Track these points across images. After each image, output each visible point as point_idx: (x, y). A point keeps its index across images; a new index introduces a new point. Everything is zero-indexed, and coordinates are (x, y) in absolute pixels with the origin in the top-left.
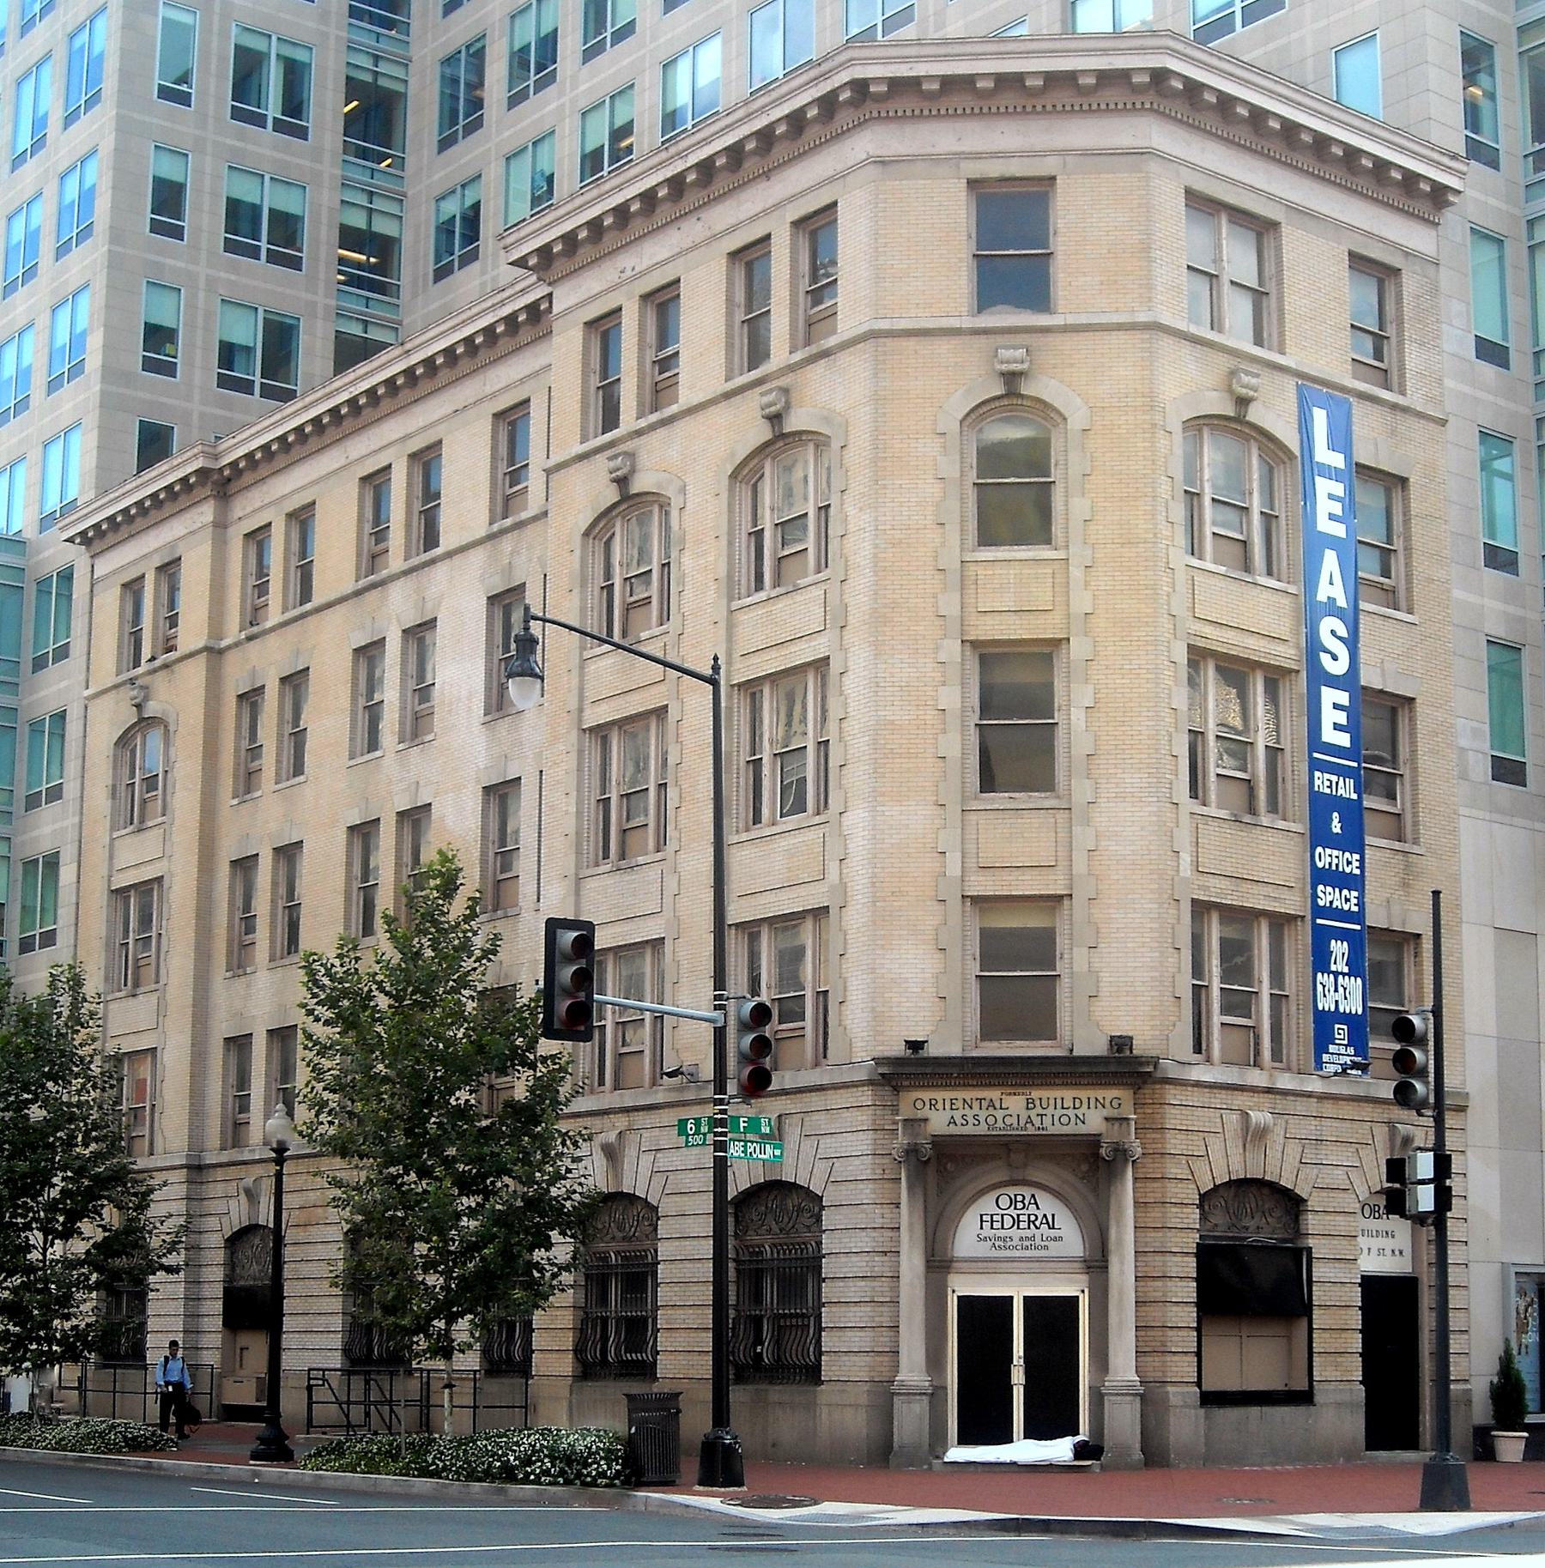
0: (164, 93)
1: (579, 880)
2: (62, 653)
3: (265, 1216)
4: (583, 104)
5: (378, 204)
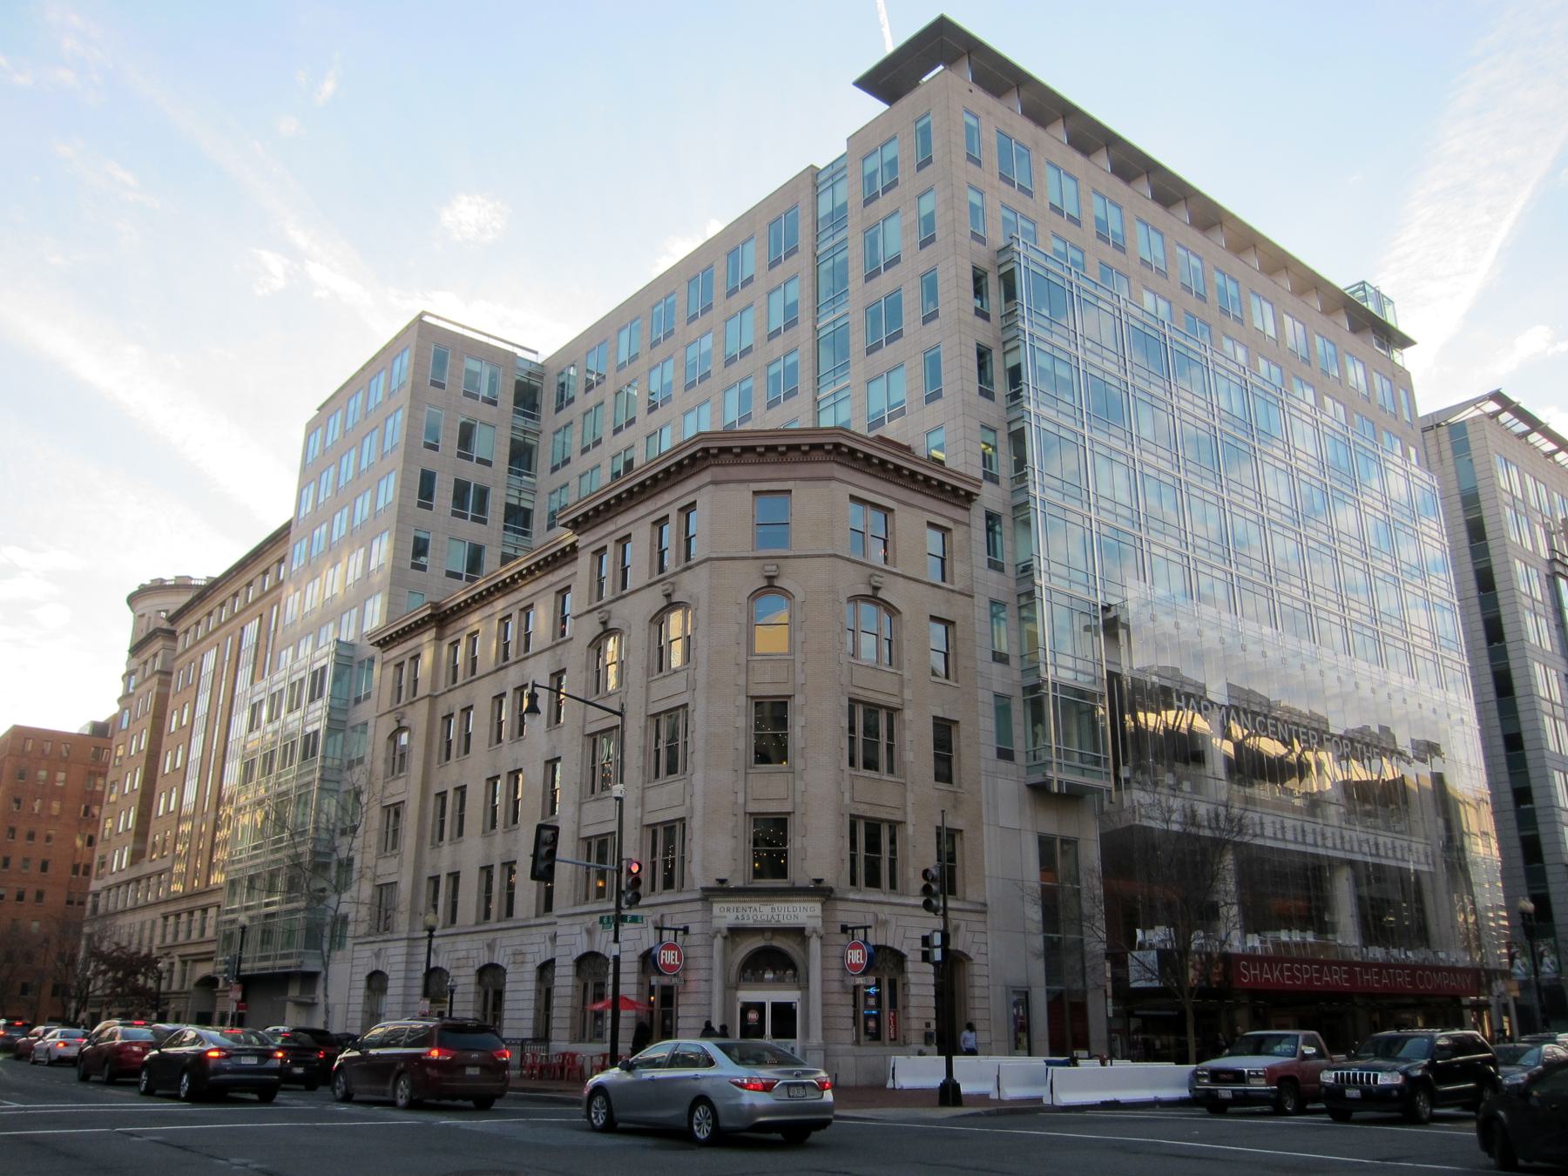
1: (581, 804)
2: (368, 696)
4: (613, 453)
5: (524, 496)
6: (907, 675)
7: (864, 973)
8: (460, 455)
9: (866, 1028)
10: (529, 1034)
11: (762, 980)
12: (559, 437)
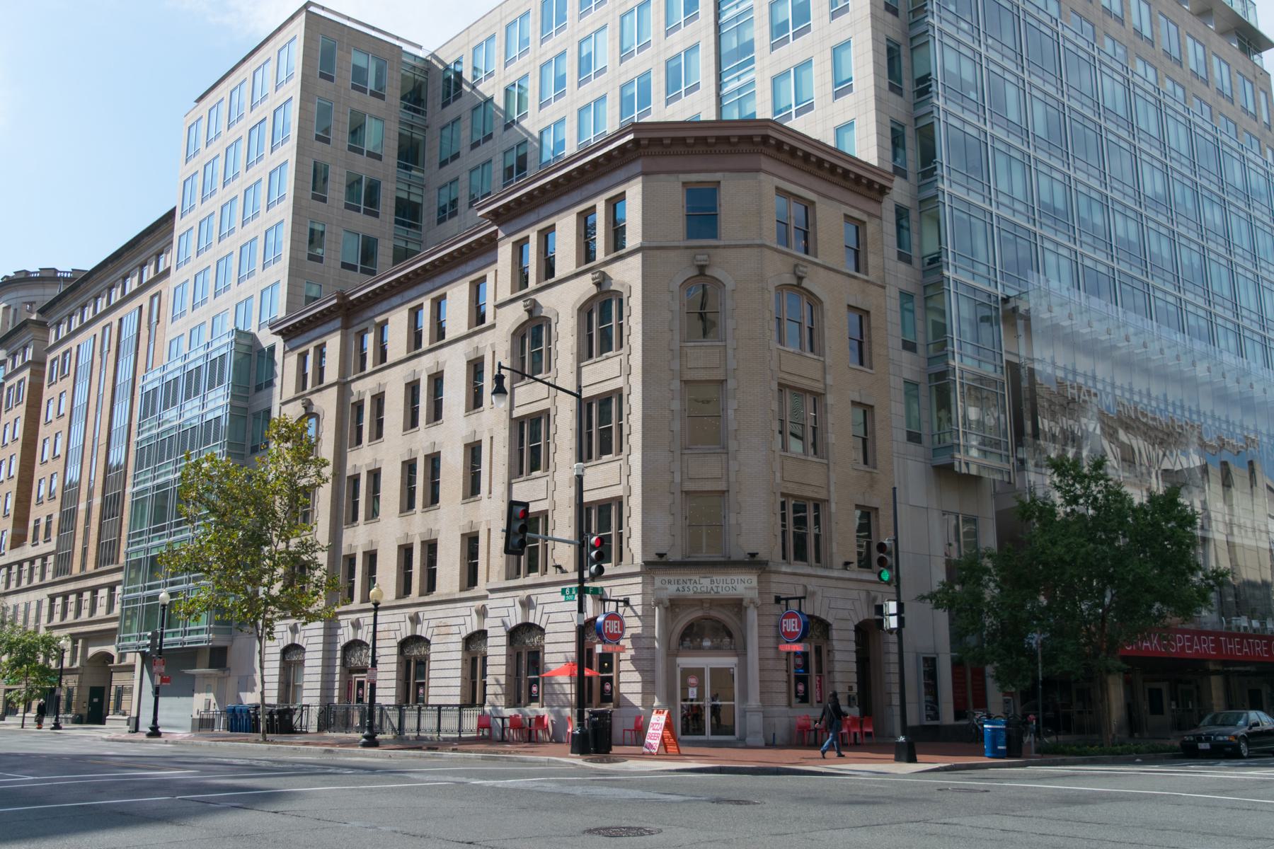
0: (318, 138)
3: (365, 635)
4: (505, 147)
5: (413, 190)
6: (828, 361)
7: (799, 641)
8: (351, 149)
9: (797, 692)
10: (457, 701)
11: (700, 648)
12: (447, 133)
